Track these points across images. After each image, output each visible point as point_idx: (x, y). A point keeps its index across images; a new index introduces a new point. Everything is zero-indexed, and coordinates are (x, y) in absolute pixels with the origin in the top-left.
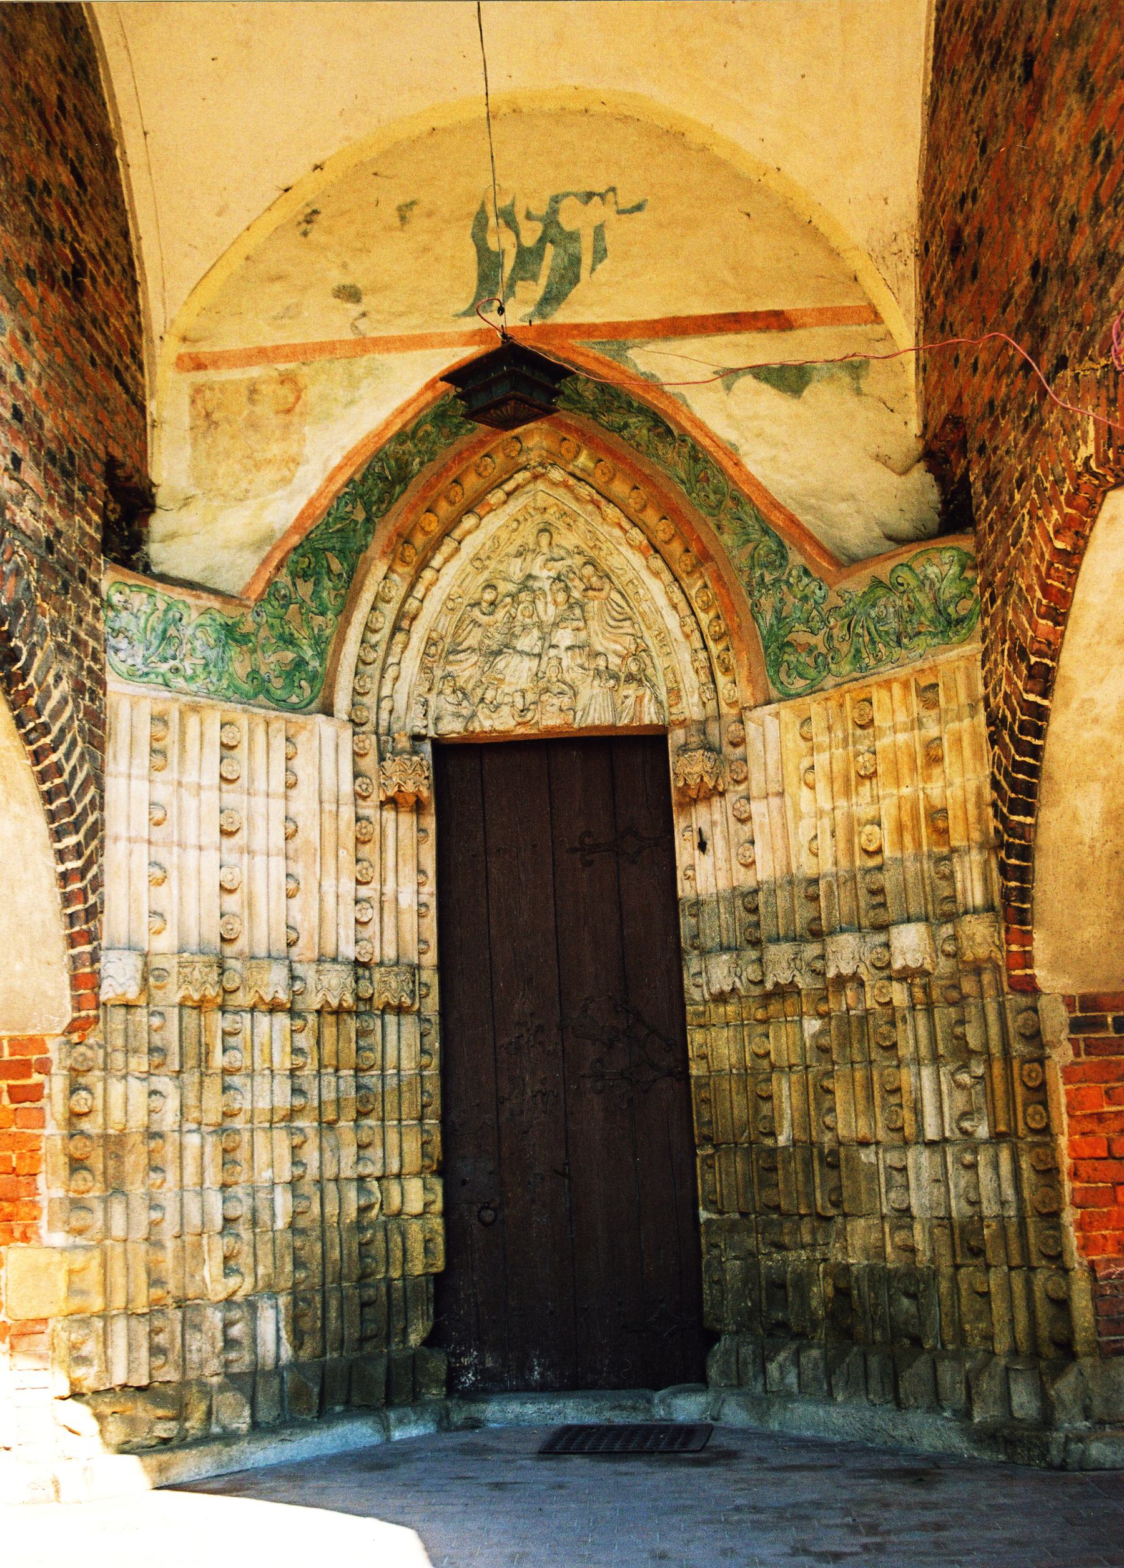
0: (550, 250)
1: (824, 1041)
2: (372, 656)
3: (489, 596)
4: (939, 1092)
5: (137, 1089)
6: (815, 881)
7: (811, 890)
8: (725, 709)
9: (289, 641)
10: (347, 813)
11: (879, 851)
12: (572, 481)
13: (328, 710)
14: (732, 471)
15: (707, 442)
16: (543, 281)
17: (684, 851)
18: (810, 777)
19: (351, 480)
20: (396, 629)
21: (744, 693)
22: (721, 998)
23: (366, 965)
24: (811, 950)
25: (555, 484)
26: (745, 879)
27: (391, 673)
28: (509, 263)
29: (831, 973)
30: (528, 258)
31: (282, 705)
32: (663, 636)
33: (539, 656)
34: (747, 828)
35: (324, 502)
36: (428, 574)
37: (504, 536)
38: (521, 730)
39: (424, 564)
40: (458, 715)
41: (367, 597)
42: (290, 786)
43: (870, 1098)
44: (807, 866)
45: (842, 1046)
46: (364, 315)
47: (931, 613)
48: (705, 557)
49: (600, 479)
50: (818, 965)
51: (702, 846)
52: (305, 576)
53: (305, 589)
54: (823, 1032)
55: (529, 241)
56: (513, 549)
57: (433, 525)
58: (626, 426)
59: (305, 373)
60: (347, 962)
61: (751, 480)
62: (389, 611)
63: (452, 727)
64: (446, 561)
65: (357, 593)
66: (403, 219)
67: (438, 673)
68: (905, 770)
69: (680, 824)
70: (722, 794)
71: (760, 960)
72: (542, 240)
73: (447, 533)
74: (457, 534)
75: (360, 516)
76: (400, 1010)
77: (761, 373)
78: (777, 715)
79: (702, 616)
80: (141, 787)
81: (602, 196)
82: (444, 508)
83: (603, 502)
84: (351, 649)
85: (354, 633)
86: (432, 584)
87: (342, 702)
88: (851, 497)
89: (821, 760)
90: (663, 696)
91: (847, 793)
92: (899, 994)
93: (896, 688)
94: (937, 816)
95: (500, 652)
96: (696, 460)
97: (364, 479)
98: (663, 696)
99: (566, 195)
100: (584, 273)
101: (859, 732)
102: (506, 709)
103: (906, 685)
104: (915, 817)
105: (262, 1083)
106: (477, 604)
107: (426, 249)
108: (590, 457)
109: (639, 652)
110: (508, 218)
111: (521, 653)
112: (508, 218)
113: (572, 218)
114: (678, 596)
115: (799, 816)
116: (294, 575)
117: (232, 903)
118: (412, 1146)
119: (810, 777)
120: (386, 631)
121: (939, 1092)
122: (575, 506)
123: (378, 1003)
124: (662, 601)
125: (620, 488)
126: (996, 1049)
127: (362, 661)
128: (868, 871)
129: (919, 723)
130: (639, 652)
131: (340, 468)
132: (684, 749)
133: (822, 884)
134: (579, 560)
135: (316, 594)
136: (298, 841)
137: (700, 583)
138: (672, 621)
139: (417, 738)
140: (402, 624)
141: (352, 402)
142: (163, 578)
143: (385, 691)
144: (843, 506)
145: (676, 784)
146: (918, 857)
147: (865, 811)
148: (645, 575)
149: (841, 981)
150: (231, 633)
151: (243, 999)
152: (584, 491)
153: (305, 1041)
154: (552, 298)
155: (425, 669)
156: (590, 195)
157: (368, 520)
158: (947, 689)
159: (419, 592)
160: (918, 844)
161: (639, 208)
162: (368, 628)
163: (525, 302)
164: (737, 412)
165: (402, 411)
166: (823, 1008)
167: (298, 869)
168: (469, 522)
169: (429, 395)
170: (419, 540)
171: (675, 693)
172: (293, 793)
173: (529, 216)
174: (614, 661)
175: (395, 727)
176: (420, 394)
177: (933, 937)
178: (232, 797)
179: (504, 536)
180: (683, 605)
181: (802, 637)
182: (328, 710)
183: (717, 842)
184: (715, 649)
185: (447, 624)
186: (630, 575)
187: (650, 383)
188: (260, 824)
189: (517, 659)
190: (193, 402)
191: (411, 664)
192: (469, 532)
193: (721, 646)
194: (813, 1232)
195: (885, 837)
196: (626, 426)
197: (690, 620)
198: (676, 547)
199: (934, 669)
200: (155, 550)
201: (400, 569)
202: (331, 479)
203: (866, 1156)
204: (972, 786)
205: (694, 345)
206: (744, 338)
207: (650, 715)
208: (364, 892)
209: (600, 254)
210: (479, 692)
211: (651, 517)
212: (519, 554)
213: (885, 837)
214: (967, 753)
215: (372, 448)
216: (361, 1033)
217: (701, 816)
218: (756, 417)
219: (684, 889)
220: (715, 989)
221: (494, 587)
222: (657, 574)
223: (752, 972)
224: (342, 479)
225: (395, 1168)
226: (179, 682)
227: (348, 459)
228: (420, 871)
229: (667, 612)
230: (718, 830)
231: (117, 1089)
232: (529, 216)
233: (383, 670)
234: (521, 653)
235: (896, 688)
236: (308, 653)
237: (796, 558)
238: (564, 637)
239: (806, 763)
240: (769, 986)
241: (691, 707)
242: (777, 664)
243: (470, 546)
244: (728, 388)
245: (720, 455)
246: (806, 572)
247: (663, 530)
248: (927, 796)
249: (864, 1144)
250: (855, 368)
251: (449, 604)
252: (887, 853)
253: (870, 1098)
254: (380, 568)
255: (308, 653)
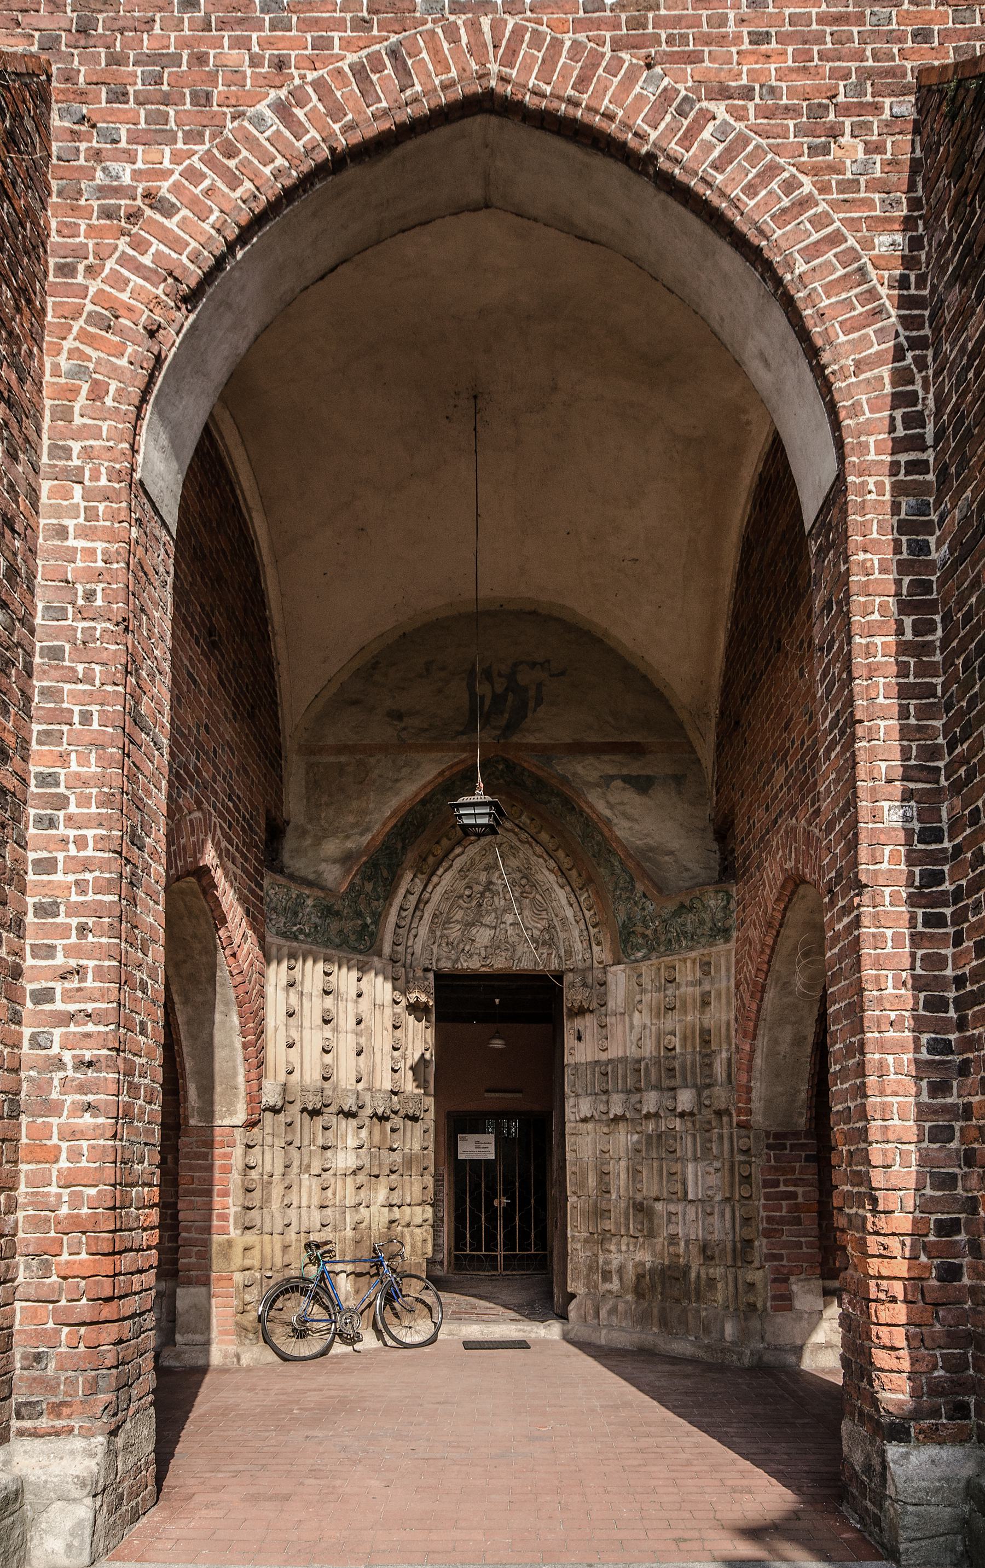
0: (510, 697)
1: (638, 1147)
2: (403, 924)
3: (467, 893)
4: (697, 1176)
5: (279, 1153)
6: (638, 1061)
7: (636, 1066)
8: (596, 964)
9: (359, 915)
10: (388, 1011)
11: (674, 1048)
12: (517, 830)
13: (380, 956)
14: (607, 834)
15: (594, 816)
16: (506, 716)
17: (569, 1040)
18: (639, 1007)
19: (395, 825)
20: (416, 908)
21: (607, 957)
22: (585, 1120)
23: (396, 1094)
24: (635, 1098)
25: (507, 830)
26: (604, 1057)
27: (413, 932)
28: (487, 702)
29: (644, 1112)
30: (498, 700)
31: (355, 950)
32: (564, 921)
33: (495, 928)
34: (604, 1031)
35: (381, 838)
36: (435, 879)
37: (478, 858)
38: (483, 969)
39: (433, 873)
40: (448, 958)
41: (402, 891)
42: (359, 995)
43: (661, 1176)
44: (632, 1052)
45: (647, 1150)
46: (404, 729)
47: (709, 925)
48: (590, 880)
49: (533, 831)
50: (638, 1106)
51: (579, 1039)
52: (369, 880)
53: (369, 887)
54: (638, 1142)
55: (499, 689)
56: (482, 866)
57: (439, 852)
58: (550, 802)
59: (372, 760)
60: (386, 1091)
61: (617, 839)
62: (413, 899)
63: (446, 965)
64: (445, 871)
65: (397, 887)
66: (427, 670)
67: (438, 933)
68: (689, 1007)
69: (567, 1025)
70: (592, 1012)
71: (607, 1102)
72: (506, 689)
73: (446, 855)
74: (451, 856)
75: (399, 846)
76: (415, 1119)
77: (627, 779)
78: (624, 971)
79: (586, 912)
80: (281, 995)
81: (542, 665)
82: (445, 842)
83: (534, 843)
84: (392, 918)
85: (394, 911)
86: (437, 884)
87: (387, 950)
88: (672, 853)
89: (646, 998)
90: (563, 954)
91: (658, 1017)
92: (677, 1124)
93: (689, 964)
94: (705, 1036)
95: (473, 925)
96: (588, 826)
97: (403, 825)
98: (563, 954)
99: (521, 663)
100: (530, 714)
101: (668, 985)
102: (475, 957)
103: (694, 962)
104: (693, 1032)
105: (341, 1155)
106: (461, 897)
107: (440, 691)
108: (528, 817)
109: (550, 928)
110: (488, 675)
111: (486, 925)
112: (488, 675)
113: (524, 678)
114: (573, 899)
115: (632, 1027)
116: (363, 879)
117: (328, 1059)
118: (417, 1188)
119: (639, 1007)
120: (411, 910)
121: (697, 1176)
122: (518, 844)
123: (402, 1113)
124: (564, 902)
125: (544, 836)
126: (726, 1155)
127: (398, 926)
128: (667, 1058)
129: (700, 983)
130: (550, 928)
131: (390, 818)
132: (572, 985)
133: (643, 1064)
134: (518, 875)
135: (374, 889)
136: (362, 1025)
137: (586, 895)
138: (569, 913)
139: (426, 970)
140: (421, 903)
141: (397, 781)
142: (291, 877)
143: (410, 943)
144: (667, 858)
145: (566, 1004)
146: (694, 1052)
147: (669, 1026)
148: (556, 887)
149: (648, 1116)
150: (328, 912)
151: (333, 1109)
152: (524, 836)
153: (364, 1133)
154: (512, 727)
155: (432, 931)
156: (533, 665)
157: (404, 848)
158: (716, 966)
159: (429, 889)
160: (694, 1048)
161: (562, 673)
162: (402, 908)
163: (495, 728)
164: (611, 799)
165: (425, 787)
166: (639, 1129)
167: (363, 1041)
168: (458, 850)
169: (440, 780)
170: (431, 860)
171: (569, 953)
172: (360, 999)
173: (500, 675)
174: (536, 933)
175: (414, 964)
176: (435, 778)
177: (699, 1095)
178: (329, 1001)
179: (478, 858)
180: (576, 905)
181: (639, 929)
182: (380, 956)
183: (587, 1036)
184: (593, 931)
185: (445, 907)
186: (548, 886)
187: (564, 780)
188: (341, 1015)
189: (482, 929)
190: (308, 774)
191: (423, 931)
192: (459, 855)
193: (596, 930)
194: (628, 1245)
195: (677, 1042)
196: (550, 802)
197: (580, 914)
198: (574, 873)
199: (710, 955)
200: (286, 857)
201: (419, 876)
202: (384, 825)
203: (659, 1206)
204: (724, 1018)
205: (591, 759)
206: (618, 758)
207: (554, 965)
208: (396, 1053)
209: (539, 701)
210: (461, 946)
211: (561, 854)
212: (485, 869)
213: (677, 1042)
214: (724, 1000)
215: (408, 807)
216: (393, 1130)
217: (579, 1023)
218: (622, 803)
219: (568, 1059)
220: (582, 1116)
221: (471, 888)
222: (562, 887)
223: (602, 1108)
224: (390, 825)
225: (408, 1201)
226: (301, 937)
227: (394, 813)
228: (426, 1042)
229: (567, 907)
230: (588, 1031)
231: (268, 1157)
232: (500, 675)
233: (409, 931)
234: (486, 925)
235: (689, 964)
236: (369, 921)
237: (640, 887)
238: (509, 918)
239: (638, 998)
240: (611, 1116)
241: (578, 959)
242: (626, 941)
243: (457, 864)
244: (608, 786)
245: (601, 825)
246: (645, 895)
247: (567, 863)
248: (701, 1023)
249: (657, 1199)
250: (678, 780)
251: (446, 896)
252: (678, 1050)
253: (661, 1176)
254: (409, 876)
255: (369, 921)
